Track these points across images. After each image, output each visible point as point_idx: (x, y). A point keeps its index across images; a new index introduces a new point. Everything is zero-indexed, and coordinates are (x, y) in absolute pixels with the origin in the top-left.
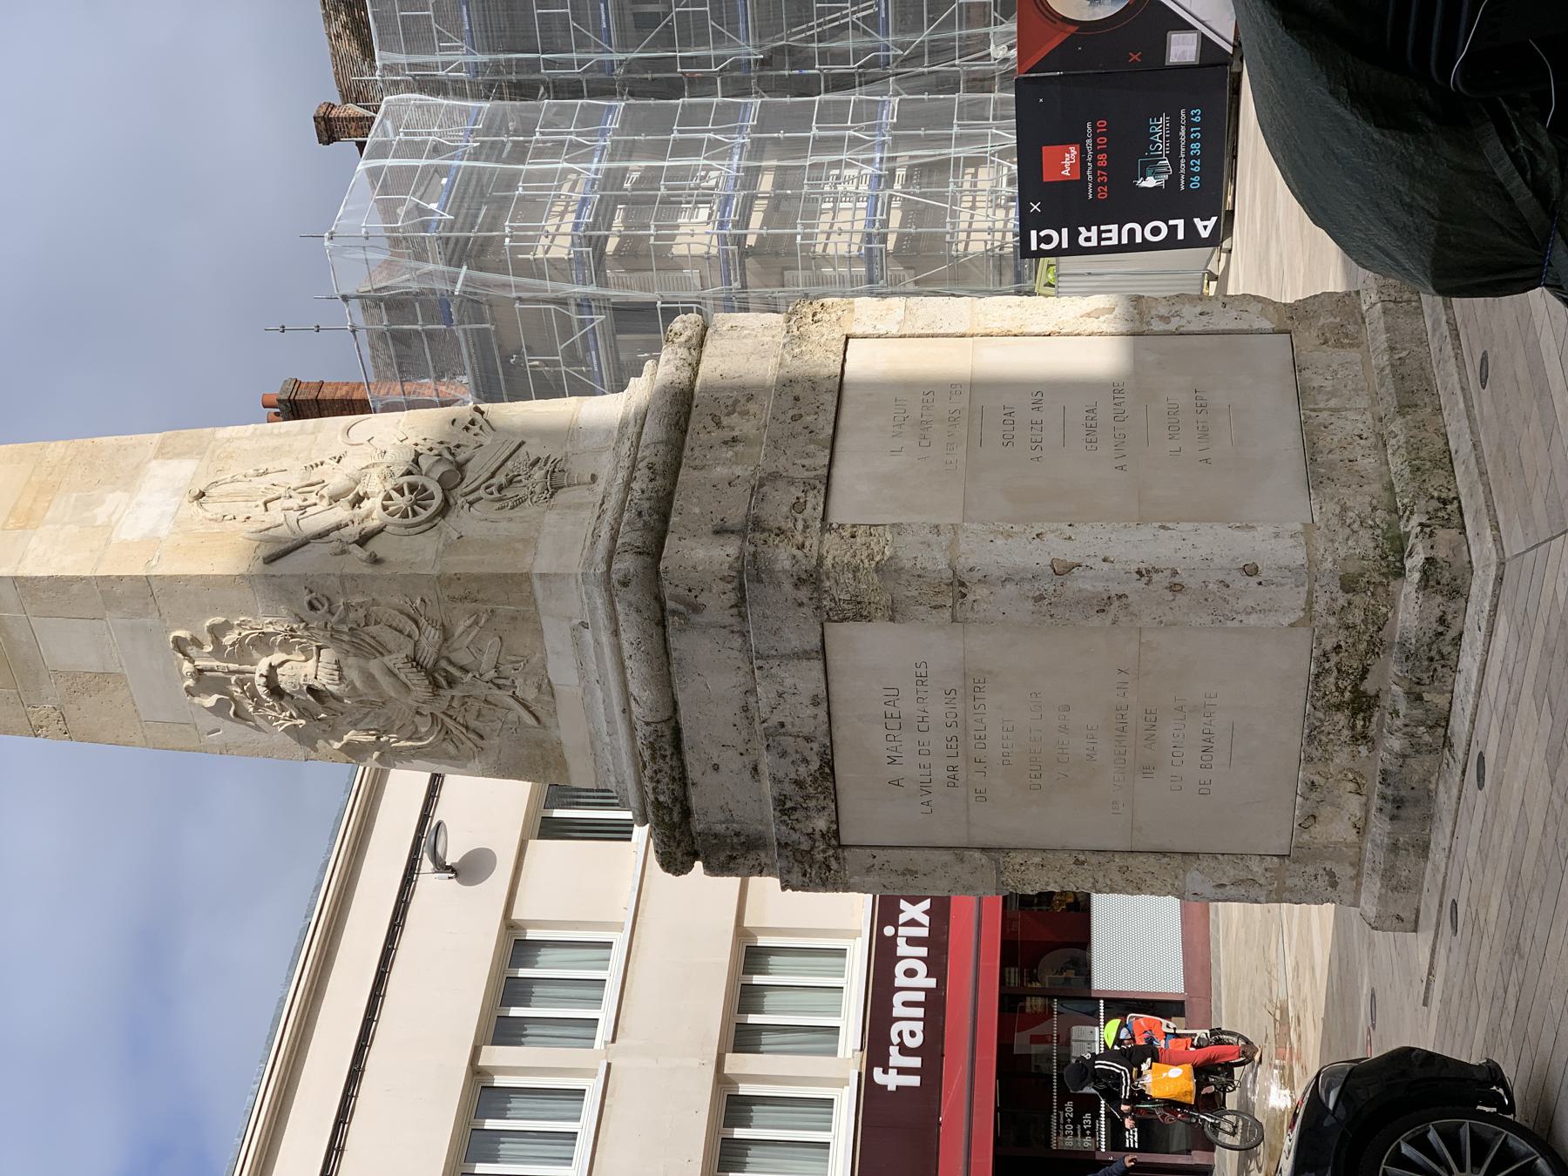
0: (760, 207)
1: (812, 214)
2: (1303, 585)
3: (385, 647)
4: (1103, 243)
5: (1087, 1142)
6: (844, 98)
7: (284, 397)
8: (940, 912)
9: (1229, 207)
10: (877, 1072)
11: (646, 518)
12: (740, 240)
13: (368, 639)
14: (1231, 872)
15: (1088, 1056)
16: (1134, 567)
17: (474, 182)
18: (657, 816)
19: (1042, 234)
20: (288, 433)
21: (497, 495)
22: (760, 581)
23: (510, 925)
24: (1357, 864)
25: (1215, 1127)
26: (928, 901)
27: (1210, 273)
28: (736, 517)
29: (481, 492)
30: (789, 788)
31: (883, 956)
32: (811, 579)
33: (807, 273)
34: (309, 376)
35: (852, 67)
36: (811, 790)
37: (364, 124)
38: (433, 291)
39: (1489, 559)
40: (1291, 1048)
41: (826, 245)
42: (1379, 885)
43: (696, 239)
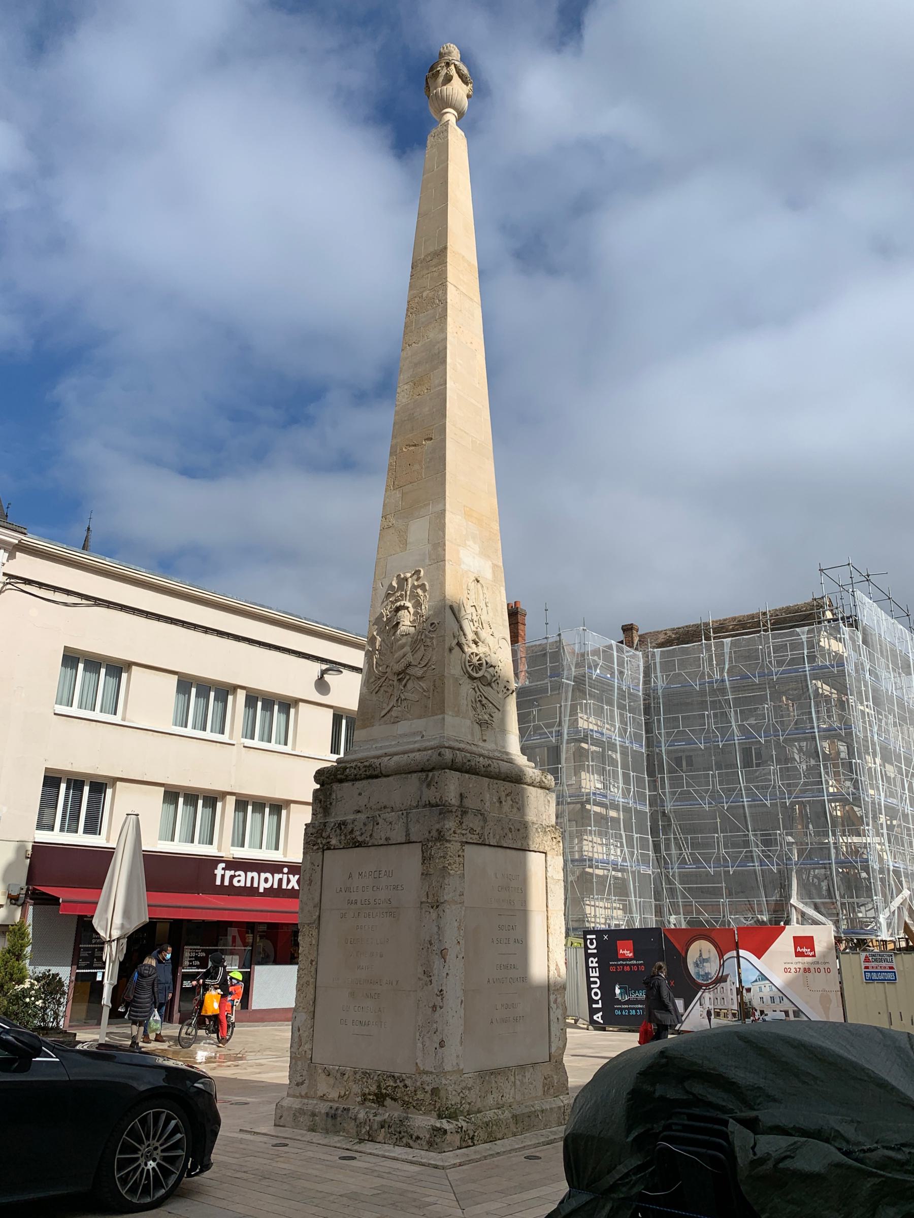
0: (603, 811)
1: (600, 834)
2: (435, 1069)
3: (414, 653)
4: (590, 969)
5: (186, 963)
6: (651, 850)
7: (519, 610)
8: (293, 893)
9: (607, 1029)
10: (223, 865)
11: (468, 763)
12: (588, 802)
13: (418, 647)
14: (305, 1035)
15: (225, 964)
16: (444, 988)
17: (609, 688)
18: (340, 768)
19: (594, 941)
20: (503, 615)
21: (478, 699)
22: (440, 814)
23: (296, 702)
24: (307, 1096)
25: (190, 1025)
26: (298, 888)
27: (578, 1020)
28: (468, 803)
29: (479, 693)
30: (350, 827)
31: (274, 867)
32: (441, 837)
33: (575, 832)
34: (527, 620)
35: (664, 853)
36: (349, 837)
37: (630, 644)
38: (563, 671)
39: (446, 1161)
40: (224, 1062)
41: (587, 840)
42: (297, 1107)
43: (588, 782)
